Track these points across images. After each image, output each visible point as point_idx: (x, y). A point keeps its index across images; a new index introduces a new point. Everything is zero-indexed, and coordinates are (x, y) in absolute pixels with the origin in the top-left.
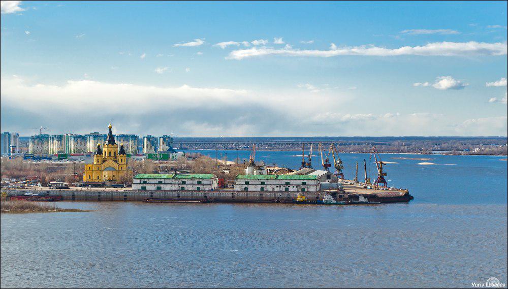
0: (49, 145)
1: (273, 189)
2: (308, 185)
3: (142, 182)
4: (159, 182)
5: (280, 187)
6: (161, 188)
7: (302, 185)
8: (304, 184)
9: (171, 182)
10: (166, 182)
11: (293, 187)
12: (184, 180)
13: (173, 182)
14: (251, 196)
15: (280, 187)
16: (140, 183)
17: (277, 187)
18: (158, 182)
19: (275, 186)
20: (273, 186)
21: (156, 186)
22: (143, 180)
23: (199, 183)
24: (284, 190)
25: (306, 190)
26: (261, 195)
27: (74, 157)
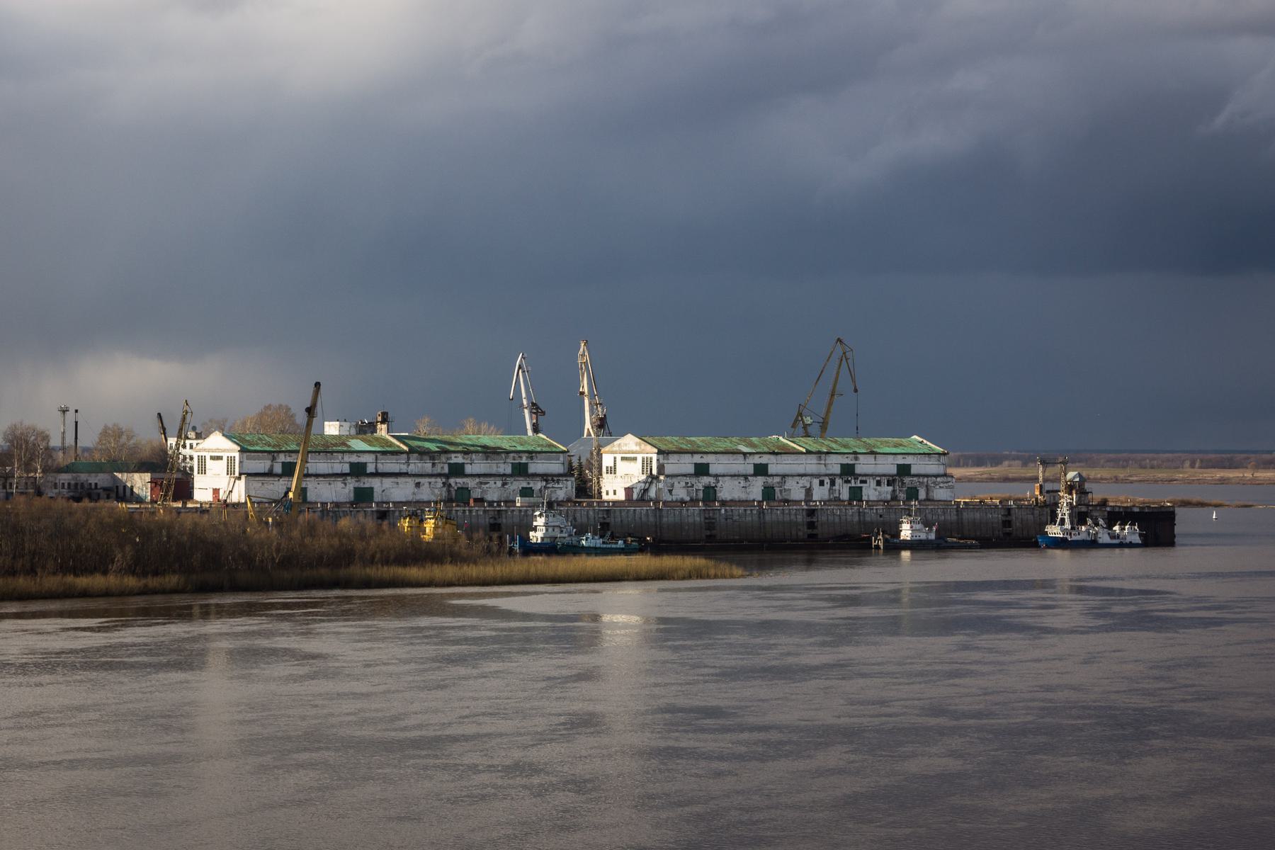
0: (428, 647)
1: (809, 491)
2: (918, 476)
3: (278, 469)
4: (352, 465)
5: (833, 483)
6: (370, 491)
7: (756, 474)
8: (904, 470)
9: (404, 468)
10: (382, 468)
11: (879, 483)
12: (459, 459)
13: (413, 468)
14: (671, 519)
15: (833, 483)
16: (270, 474)
17: (822, 483)
18: (346, 469)
19: (816, 481)
20: (805, 482)
21: (352, 483)
22: (282, 458)
23: (520, 470)
24: (845, 495)
25: (922, 495)
26: (761, 512)
27: (481, 719)
